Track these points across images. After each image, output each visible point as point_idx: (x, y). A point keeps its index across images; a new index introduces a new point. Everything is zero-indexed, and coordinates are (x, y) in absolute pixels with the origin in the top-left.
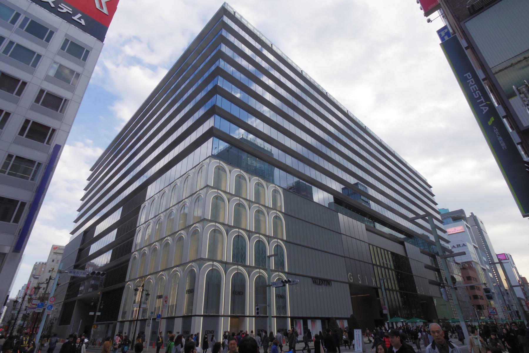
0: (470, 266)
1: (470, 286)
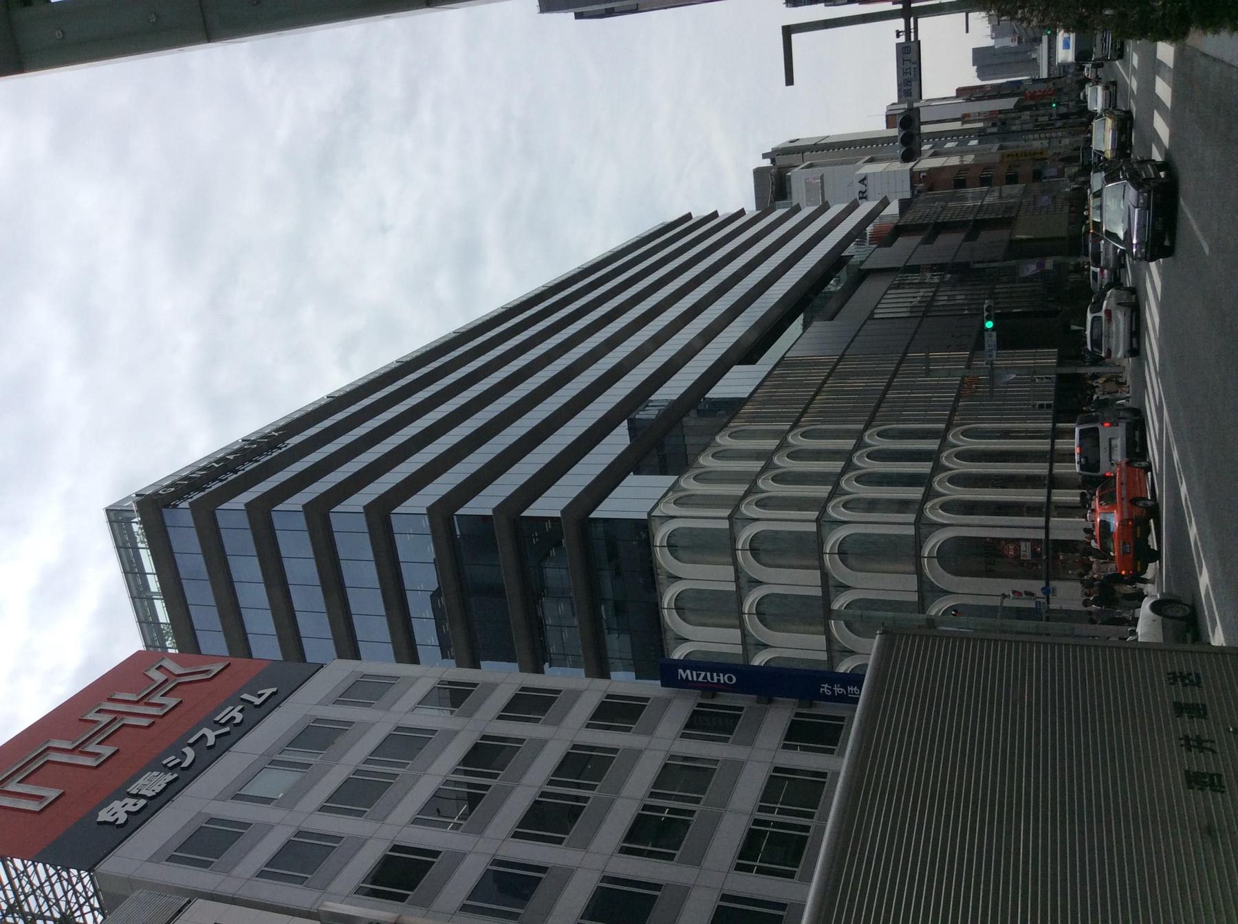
0: (923, 177)
1: (867, 665)
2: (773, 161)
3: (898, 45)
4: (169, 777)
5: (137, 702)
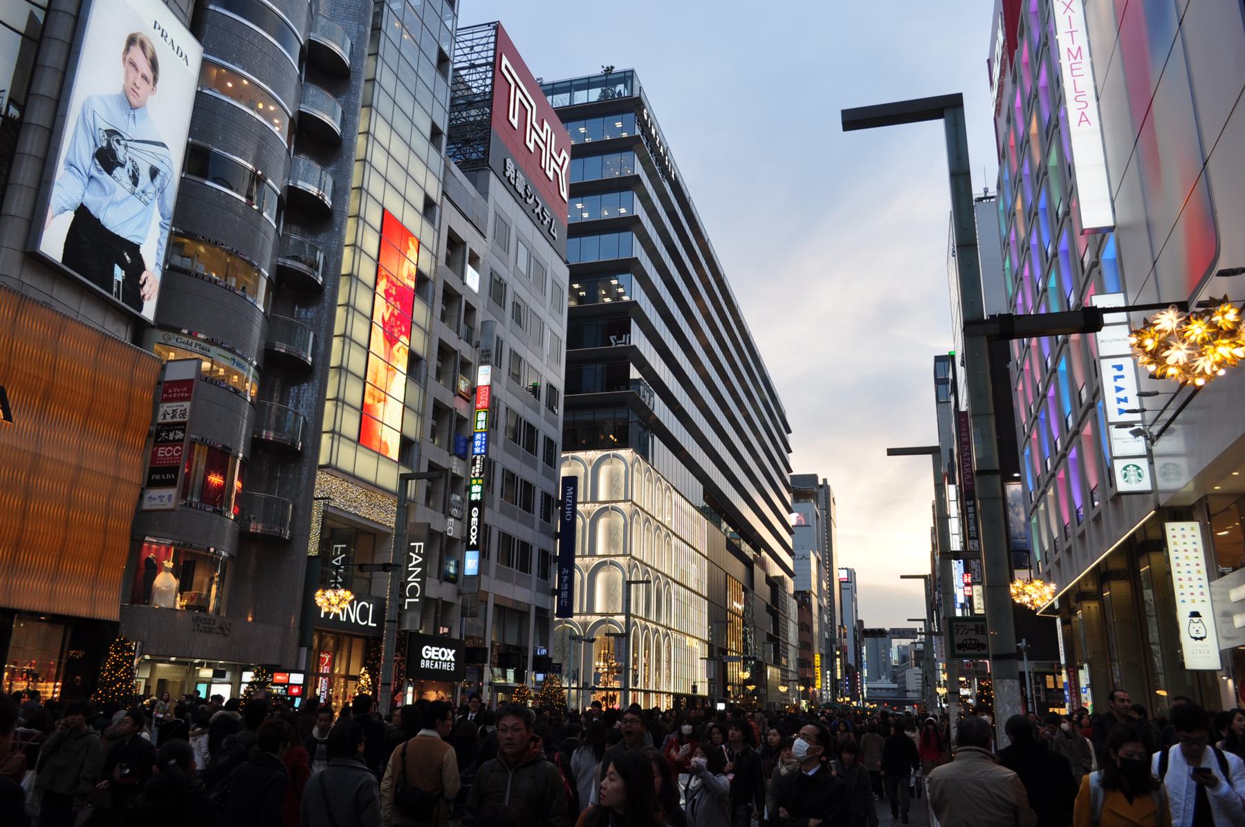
2: (821, 486)
3: (916, 629)
4: (523, 193)
5: (551, 153)
